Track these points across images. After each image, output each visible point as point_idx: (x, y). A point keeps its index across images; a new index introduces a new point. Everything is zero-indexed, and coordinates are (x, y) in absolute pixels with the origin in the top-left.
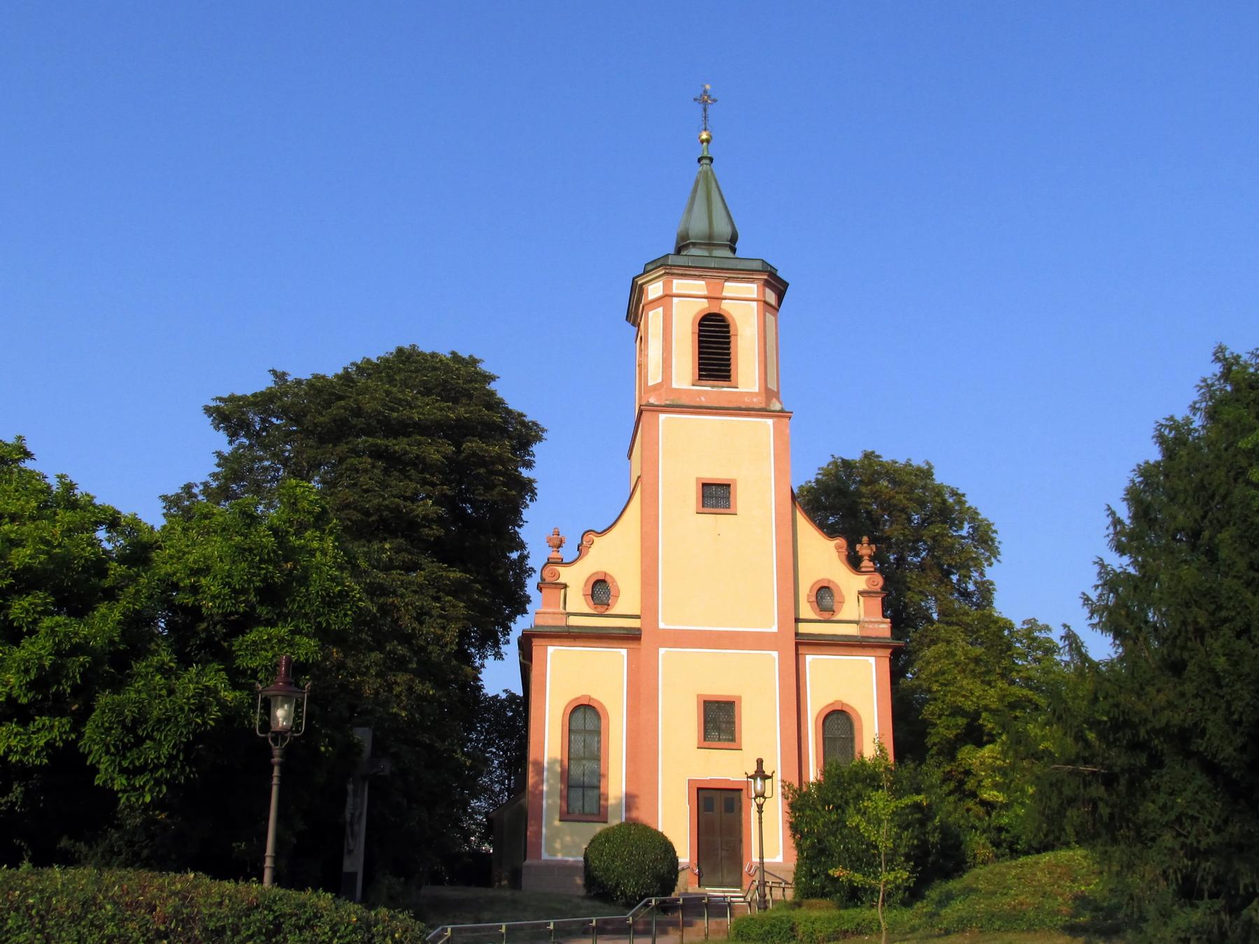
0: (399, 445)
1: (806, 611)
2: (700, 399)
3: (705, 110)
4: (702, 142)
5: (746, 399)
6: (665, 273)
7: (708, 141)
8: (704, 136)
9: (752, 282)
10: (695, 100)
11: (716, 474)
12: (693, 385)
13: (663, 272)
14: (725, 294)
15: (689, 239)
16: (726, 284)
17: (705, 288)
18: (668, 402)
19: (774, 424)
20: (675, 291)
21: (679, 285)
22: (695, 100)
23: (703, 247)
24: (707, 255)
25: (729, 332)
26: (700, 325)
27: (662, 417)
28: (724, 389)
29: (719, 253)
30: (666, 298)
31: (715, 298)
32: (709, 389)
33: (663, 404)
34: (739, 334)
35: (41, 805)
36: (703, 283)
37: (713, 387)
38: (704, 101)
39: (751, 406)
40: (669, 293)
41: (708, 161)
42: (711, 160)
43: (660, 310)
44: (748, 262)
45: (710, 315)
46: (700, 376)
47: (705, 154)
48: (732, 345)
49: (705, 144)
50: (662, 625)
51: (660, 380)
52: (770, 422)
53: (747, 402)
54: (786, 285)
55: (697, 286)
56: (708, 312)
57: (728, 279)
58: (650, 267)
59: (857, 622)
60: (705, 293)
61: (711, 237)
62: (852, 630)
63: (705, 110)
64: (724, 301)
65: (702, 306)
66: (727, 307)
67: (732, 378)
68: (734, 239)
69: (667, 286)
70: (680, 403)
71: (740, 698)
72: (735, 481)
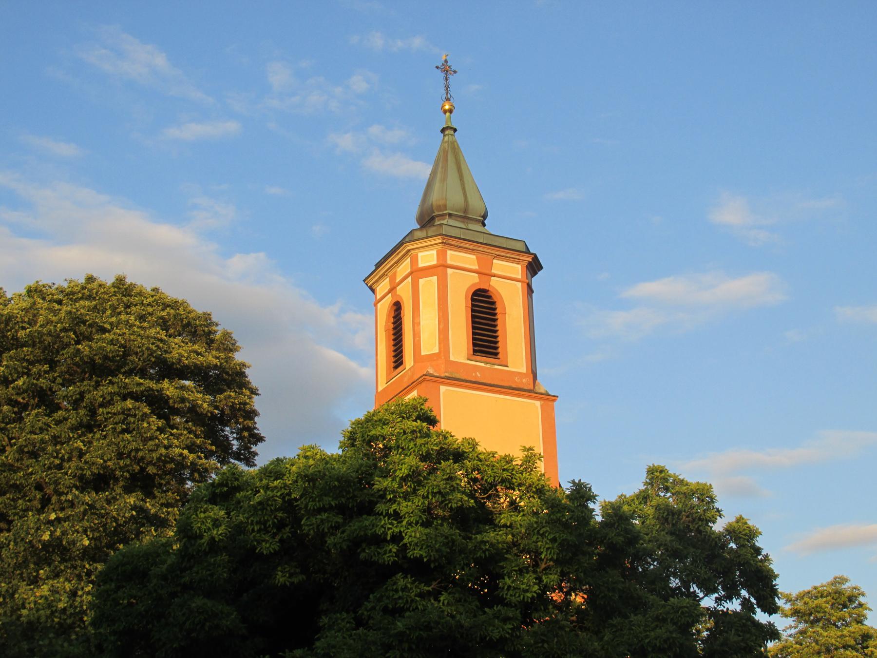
0: (169, 388)
3: (446, 80)
4: (445, 112)
5: (516, 379)
6: (442, 243)
7: (451, 111)
8: (447, 107)
9: (518, 263)
10: (437, 67)
12: (469, 359)
13: (440, 241)
14: (494, 271)
15: (446, 210)
16: (495, 261)
17: (476, 263)
18: (447, 374)
19: (542, 406)
20: (449, 262)
21: (453, 256)
22: (437, 67)
23: (459, 219)
24: (465, 227)
25: (495, 309)
26: (472, 299)
27: (443, 388)
28: (496, 367)
29: (472, 226)
31: (485, 274)
32: (482, 364)
33: (443, 375)
34: (507, 312)
35: (486, 590)
36: (474, 257)
37: (486, 363)
38: (446, 69)
39: (521, 386)
41: (452, 132)
42: (455, 130)
44: (513, 242)
45: (479, 290)
46: (474, 351)
47: (449, 125)
48: (499, 322)
49: (448, 114)
51: (436, 350)
52: (538, 404)
53: (517, 382)
54: (540, 267)
55: (469, 260)
56: (478, 287)
57: (497, 257)
60: (476, 267)
61: (466, 210)
63: (446, 80)
64: (492, 278)
65: (472, 280)
67: (500, 356)
68: (485, 216)
69: (442, 255)
70: (458, 376)
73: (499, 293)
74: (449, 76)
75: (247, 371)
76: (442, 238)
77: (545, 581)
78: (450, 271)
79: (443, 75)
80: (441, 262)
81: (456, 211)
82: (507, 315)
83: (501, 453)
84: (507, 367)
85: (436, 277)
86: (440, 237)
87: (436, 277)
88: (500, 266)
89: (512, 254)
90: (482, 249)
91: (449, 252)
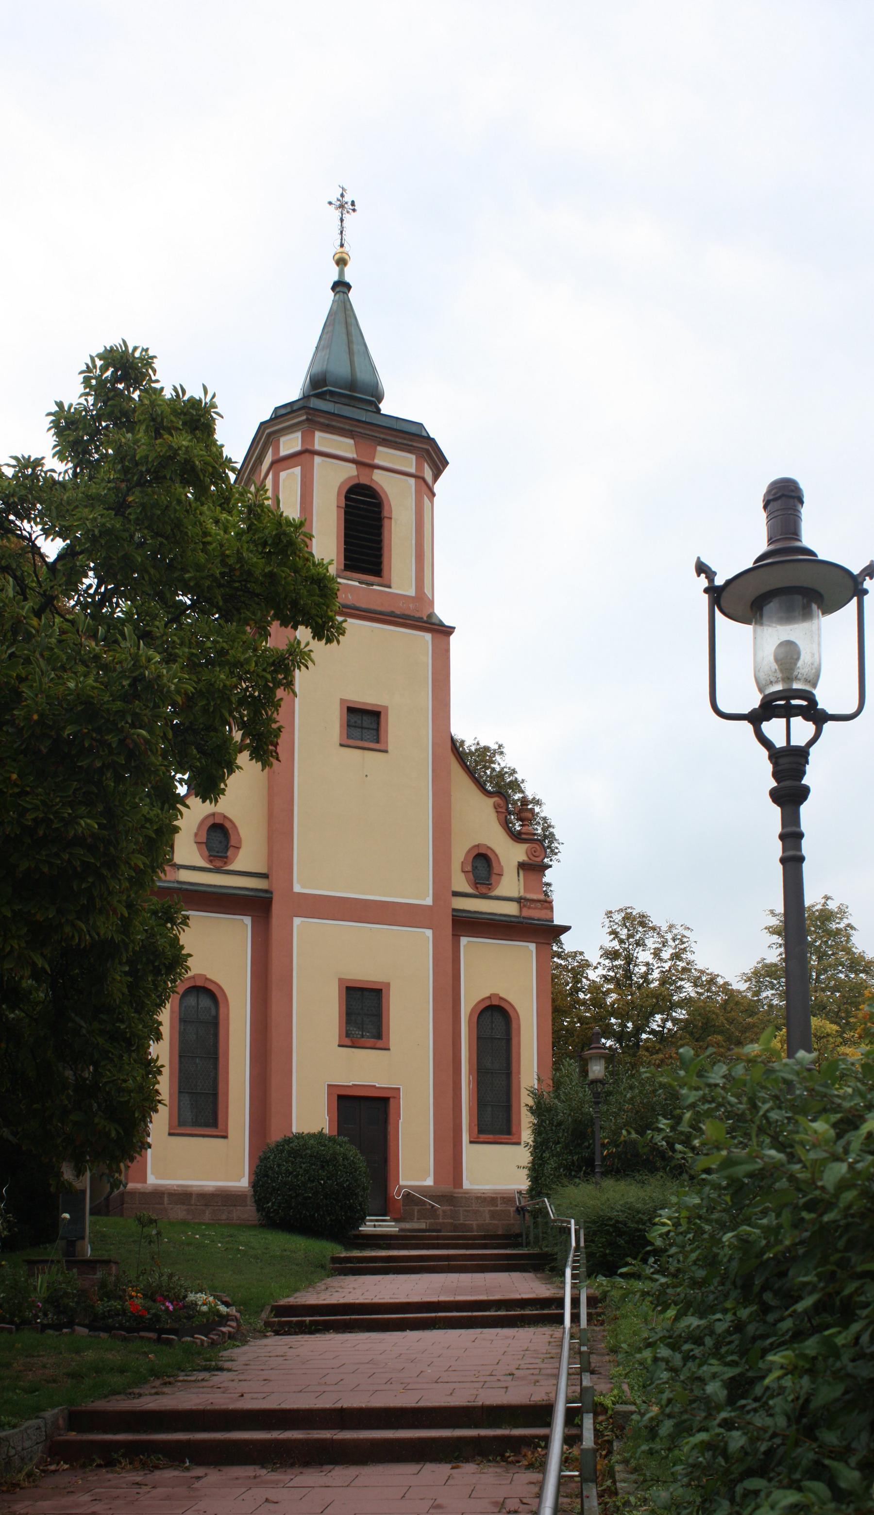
1: (461, 883)
2: (347, 597)
10: (330, 203)
11: (367, 698)
13: (304, 417)
14: (377, 461)
15: (326, 386)
20: (317, 447)
21: (322, 441)
22: (330, 203)
26: (347, 498)
28: (375, 587)
30: (307, 455)
32: (357, 584)
34: (394, 516)
40: (309, 447)
43: (297, 470)
46: (346, 565)
50: (297, 888)
52: (428, 636)
53: (400, 608)
55: (344, 446)
56: (356, 481)
58: (283, 411)
59: (519, 900)
60: (351, 455)
62: (511, 909)
63: (342, 220)
64: (376, 471)
65: (351, 470)
66: (380, 479)
71: (388, 985)
72: (386, 708)
73: (385, 492)
74: (346, 217)
75: (767, 961)
76: (307, 414)
77: (116, 739)
78: (317, 459)
79: (337, 214)
80: (304, 448)
81: (340, 388)
82: (393, 521)
83: (530, 792)
84: (389, 587)
85: (299, 468)
86: (303, 411)
87: (299, 468)
88: (385, 456)
89: (404, 439)
90: (362, 431)
91: (318, 435)
